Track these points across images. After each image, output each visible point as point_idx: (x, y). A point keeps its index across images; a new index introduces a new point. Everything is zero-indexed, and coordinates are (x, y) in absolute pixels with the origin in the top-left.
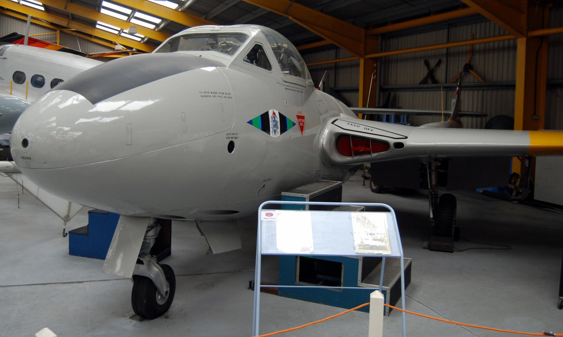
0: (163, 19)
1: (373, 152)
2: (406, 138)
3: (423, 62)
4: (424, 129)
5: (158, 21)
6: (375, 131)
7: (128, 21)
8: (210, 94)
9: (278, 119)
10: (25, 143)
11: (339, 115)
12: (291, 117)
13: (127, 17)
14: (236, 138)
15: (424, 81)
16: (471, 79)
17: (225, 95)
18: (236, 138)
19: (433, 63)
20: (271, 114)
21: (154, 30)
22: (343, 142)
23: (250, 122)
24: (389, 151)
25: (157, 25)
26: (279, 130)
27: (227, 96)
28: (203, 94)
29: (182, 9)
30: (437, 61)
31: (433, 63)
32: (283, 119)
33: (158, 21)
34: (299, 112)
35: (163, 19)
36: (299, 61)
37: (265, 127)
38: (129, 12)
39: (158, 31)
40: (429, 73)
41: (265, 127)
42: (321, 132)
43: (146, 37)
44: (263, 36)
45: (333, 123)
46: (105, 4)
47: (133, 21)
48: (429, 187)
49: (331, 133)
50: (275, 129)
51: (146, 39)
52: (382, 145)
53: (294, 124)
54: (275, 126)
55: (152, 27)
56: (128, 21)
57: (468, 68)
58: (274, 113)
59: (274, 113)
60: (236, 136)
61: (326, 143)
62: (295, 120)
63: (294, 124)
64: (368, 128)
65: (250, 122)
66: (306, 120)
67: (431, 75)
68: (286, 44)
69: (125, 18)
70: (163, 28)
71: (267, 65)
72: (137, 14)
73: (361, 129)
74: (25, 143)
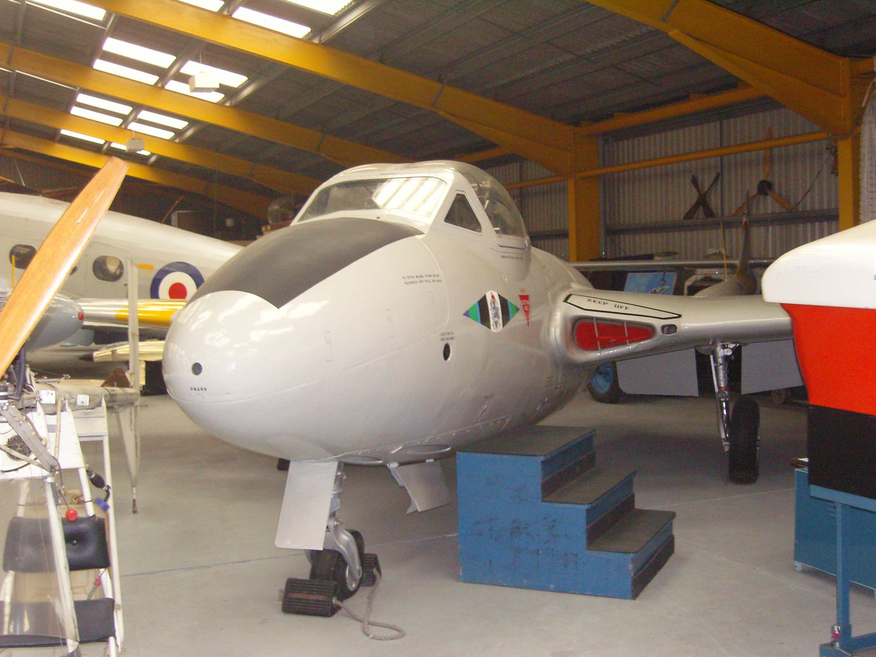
0: (192, 122)
1: (630, 342)
2: (680, 316)
3: (688, 180)
4: (703, 299)
5: (181, 124)
6: (632, 310)
7: (123, 127)
8: (416, 279)
9: (498, 305)
10: (197, 369)
11: (569, 287)
12: (514, 301)
13: (121, 121)
14: (452, 339)
15: (689, 215)
16: (769, 206)
17: (432, 278)
18: (452, 339)
19: (706, 181)
20: (489, 299)
21: (172, 140)
22: (584, 331)
23: (467, 314)
24: (655, 338)
25: (178, 133)
26: (501, 321)
27: (436, 279)
28: (408, 280)
29: (325, 37)
30: (713, 176)
31: (706, 181)
32: (504, 302)
33: (181, 124)
34: (523, 291)
35: (192, 122)
36: (509, 208)
37: (484, 319)
38: (126, 110)
39: (181, 143)
40: (699, 198)
41: (484, 319)
42: (550, 317)
43: (152, 154)
44: (463, 180)
45: (566, 300)
46: (81, 98)
47: (134, 126)
48: (717, 390)
49: (565, 319)
50: (496, 319)
51: (189, 133)
52: (642, 331)
53: (518, 309)
54: (496, 315)
55: (169, 135)
56: (123, 127)
57: (765, 187)
58: (493, 297)
59: (493, 297)
60: (452, 336)
61: (561, 335)
62: (518, 303)
63: (518, 309)
64: (620, 304)
65: (467, 314)
66: (531, 302)
67: (702, 201)
68: (488, 182)
69: (118, 122)
70: (192, 137)
71: (472, 223)
72: (144, 115)
73: (610, 307)
74: (197, 369)
